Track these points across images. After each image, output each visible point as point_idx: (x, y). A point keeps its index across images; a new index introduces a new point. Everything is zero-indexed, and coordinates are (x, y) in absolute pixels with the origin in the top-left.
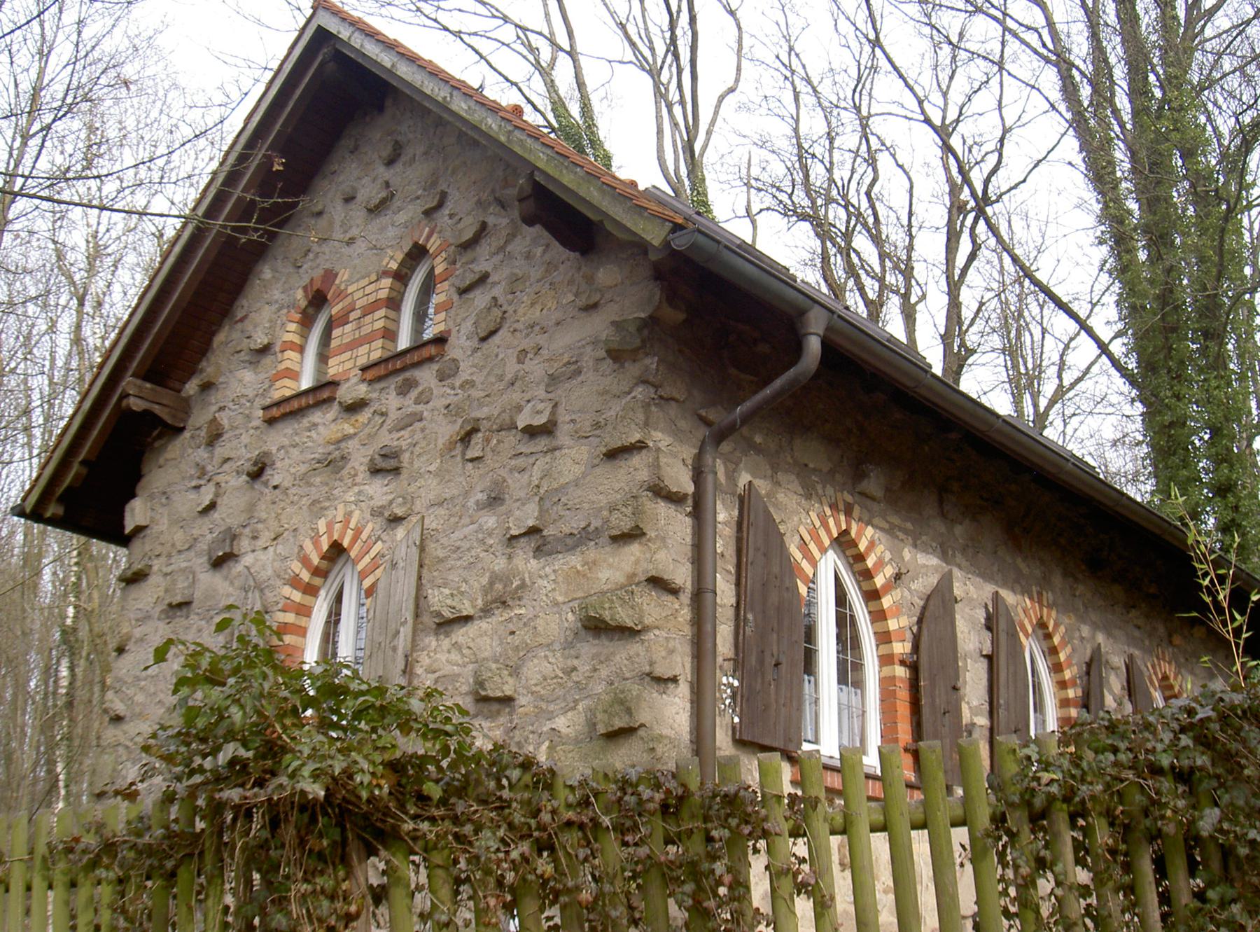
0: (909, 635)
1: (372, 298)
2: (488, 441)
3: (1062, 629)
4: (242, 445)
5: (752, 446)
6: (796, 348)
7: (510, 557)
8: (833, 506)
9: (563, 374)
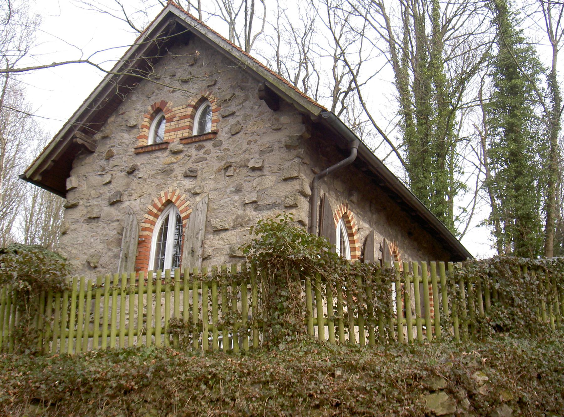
0: (360, 249)
1: (184, 114)
2: (235, 170)
3: (400, 254)
4: (124, 160)
5: (324, 182)
6: (348, 153)
7: (244, 210)
8: (343, 204)
9: (266, 151)
